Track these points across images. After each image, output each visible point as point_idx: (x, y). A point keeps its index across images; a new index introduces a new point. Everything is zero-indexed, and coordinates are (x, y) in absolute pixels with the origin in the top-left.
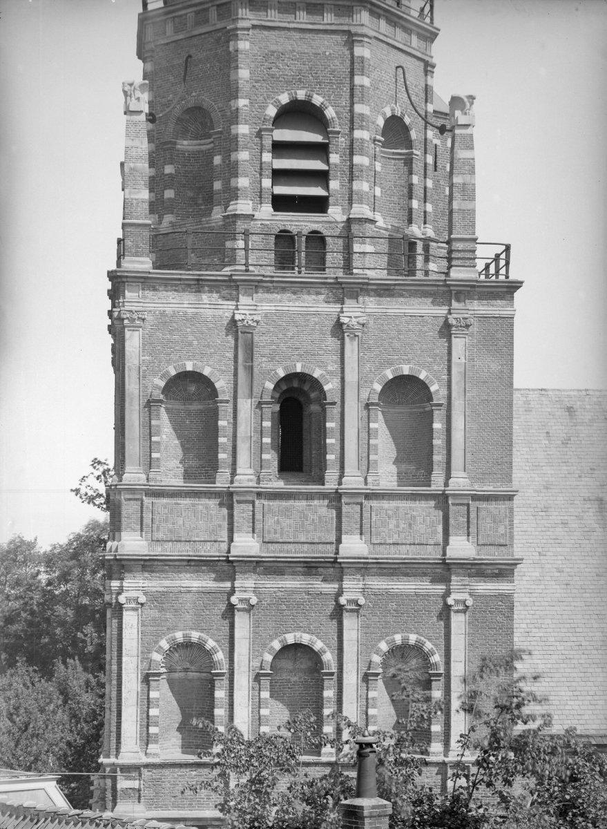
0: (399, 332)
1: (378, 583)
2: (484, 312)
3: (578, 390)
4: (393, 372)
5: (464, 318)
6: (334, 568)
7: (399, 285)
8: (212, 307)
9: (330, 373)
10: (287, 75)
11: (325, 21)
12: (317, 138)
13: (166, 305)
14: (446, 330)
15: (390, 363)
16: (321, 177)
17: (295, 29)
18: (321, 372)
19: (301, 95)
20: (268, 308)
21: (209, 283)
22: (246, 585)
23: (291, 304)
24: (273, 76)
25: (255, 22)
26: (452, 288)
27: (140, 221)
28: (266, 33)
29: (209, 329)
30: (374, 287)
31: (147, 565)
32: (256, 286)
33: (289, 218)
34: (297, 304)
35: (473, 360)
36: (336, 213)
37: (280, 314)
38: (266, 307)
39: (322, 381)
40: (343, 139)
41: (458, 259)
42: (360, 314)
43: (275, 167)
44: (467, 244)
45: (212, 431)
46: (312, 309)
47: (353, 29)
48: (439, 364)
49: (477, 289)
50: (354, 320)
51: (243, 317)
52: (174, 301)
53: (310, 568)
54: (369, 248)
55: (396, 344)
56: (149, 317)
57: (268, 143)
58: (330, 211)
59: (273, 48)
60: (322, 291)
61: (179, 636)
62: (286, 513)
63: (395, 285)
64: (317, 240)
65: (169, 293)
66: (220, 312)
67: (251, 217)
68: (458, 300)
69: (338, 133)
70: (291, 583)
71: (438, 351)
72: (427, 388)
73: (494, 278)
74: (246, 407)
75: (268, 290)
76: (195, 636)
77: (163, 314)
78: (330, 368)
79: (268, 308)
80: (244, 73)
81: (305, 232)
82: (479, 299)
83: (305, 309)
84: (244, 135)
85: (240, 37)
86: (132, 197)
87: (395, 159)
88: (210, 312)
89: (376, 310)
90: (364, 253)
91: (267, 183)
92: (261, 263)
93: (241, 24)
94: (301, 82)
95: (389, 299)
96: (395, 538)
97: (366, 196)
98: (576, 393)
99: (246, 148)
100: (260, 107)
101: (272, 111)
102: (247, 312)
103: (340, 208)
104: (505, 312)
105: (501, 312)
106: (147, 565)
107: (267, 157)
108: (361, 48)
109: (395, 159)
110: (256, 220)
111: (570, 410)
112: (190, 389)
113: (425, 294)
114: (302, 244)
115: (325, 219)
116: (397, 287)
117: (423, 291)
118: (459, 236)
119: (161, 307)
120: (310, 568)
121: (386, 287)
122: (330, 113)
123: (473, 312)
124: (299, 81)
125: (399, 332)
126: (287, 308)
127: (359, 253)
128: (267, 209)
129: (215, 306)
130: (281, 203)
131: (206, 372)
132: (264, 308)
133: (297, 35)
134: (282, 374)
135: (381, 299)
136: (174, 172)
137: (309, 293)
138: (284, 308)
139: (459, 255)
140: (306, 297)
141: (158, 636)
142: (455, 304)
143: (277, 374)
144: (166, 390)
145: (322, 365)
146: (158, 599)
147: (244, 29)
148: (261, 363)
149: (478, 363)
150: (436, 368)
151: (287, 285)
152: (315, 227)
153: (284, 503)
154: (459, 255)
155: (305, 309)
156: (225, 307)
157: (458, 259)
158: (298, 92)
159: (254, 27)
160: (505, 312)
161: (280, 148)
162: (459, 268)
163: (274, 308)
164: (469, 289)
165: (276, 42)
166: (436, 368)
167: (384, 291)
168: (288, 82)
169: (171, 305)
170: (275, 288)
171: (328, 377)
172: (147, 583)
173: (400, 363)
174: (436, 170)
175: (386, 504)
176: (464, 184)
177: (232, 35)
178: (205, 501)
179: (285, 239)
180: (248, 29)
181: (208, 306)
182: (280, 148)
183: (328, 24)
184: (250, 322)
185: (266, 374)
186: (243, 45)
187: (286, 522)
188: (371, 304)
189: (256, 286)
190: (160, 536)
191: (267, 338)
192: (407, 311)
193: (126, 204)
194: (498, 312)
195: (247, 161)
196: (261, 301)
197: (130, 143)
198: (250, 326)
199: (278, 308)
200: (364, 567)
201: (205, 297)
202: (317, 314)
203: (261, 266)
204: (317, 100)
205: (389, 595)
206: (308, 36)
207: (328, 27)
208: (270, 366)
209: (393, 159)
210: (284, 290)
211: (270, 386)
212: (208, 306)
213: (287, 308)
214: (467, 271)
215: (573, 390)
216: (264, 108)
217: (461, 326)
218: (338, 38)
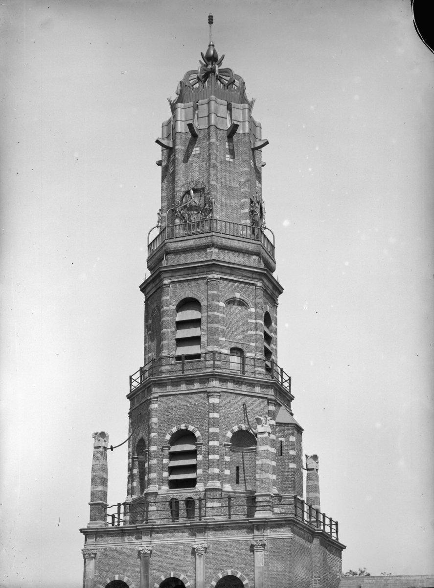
0: (226, 551)
2: (273, 536)
3: (422, 576)
4: (222, 574)
5: (260, 541)
7: (225, 524)
8: (129, 544)
9: (189, 577)
10: (176, 418)
11: (195, 388)
13: (107, 545)
14: (252, 548)
15: (221, 569)
17: (180, 394)
18: (184, 576)
19: (183, 427)
20: (157, 542)
21: (128, 531)
23: (169, 539)
24: (169, 419)
25: (160, 394)
26: (254, 524)
27: (96, 502)
28: (166, 398)
29: (128, 556)
30: (212, 526)
32: (151, 531)
33: (175, 492)
34: (172, 539)
35: (268, 564)
36: (200, 487)
37: (164, 545)
38: (156, 542)
39: (184, 582)
40: (204, 447)
41: (260, 506)
42: (203, 542)
43: (170, 465)
44: (264, 498)
46: (179, 541)
47: (208, 390)
48: (248, 568)
49: (268, 523)
50: (200, 545)
51: (143, 548)
52: (111, 543)
54: (155, 508)
55: (225, 558)
56: (99, 553)
57: (166, 453)
58: (196, 486)
59: (169, 405)
60: (185, 530)
63: (223, 524)
64: (190, 502)
65: (109, 538)
66: (133, 547)
67: (156, 494)
68: (258, 529)
69: (202, 444)
71: (248, 560)
72: (221, 580)
73: (110, 526)
75: (157, 533)
77: (105, 550)
78: (189, 574)
79: (157, 542)
80: (154, 420)
81: (184, 499)
82: (271, 528)
83: (176, 541)
84: (154, 451)
85: (153, 402)
86: (94, 490)
87: (249, 452)
88: (128, 547)
89: (214, 539)
90: (213, 507)
91: (165, 474)
92: (161, 517)
93: (154, 396)
94: (183, 420)
95: (220, 532)
98: (419, 578)
100: (163, 436)
101: (168, 437)
102: (145, 546)
103: (203, 483)
104: (285, 535)
105: (283, 536)
107: (166, 461)
108: (213, 399)
109: (249, 452)
110: (159, 495)
114: (182, 505)
115: (194, 490)
116: (224, 526)
117: (277, 524)
118: (260, 494)
119: (104, 546)
121: (218, 526)
123: (267, 537)
124: (183, 421)
125: (226, 551)
126: (166, 542)
127: (211, 508)
128: (165, 488)
129: (131, 543)
130: (174, 484)
132: (155, 542)
134: (163, 578)
135: (217, 532)
136: (296, 455)
137: (178, 532)
138: (164, 542)
139: (260, 504)
140: (176, 534)
143: (161, 579)
145: (185, 572)
147: (154, 398)
149: (271, 566)
150: (247, 570)
151: (167, 529)
152: (189, 495)
154: (260, 504)
155: (176, 541)
156: (136, 543)
157: (260, 506)
158: (182, 425)
159: (160, 396)
160: (285, 535)
161: (174, 456)
162: (260, 512)
163: (160, 542)
164: (263, 523)
165: (171, 402)
166: (247, 570)
168: (177, 421)
169: (109, 545)
170: (161, 531)
171: (187, 579)
173: (227, 569)
174: (282, 455)
176: (262, 464)
177: (149, 402)
179: (174, 504)
180: (157, 398)
181: (127, 544)
182: (174, 456)
183: (196, 389)
184: (146, 551)
186: (154, 406)
188: (211, 536)
189: (151, 531)
191: (156, 559)
192: (230, 538)
193: (92, 494)
194: (281, 535)
195: (156, 464)
196: (154, 539)
197: (95, 463)
198: (146, 553)
199: (163, 542)
201: (126, 539)
202: (182, 544)
203: (161, 519)
204: (191, 428)
206: (187, 396)
207: (196, 391)
208: (157, 575)
209: (249, 452)
210: (165, 532)
212: (127, 544)
213: (166, 542)
214: (264, 513)
215: (419, 576)
216: (164, 436)
217: (259, 545)
218: (202, 395)
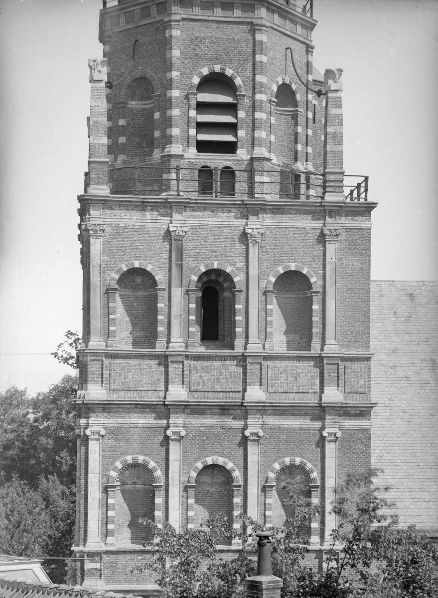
0: (288, 239)
1: (273, 421)
2: (349, 225)
3: (417, 282)
4: (283, 268)
5: (335, 230)
6: (241, 410)
7: (288, 205)
8: (153, 221)
9: (238, 269)
10: (207, 54)
11: (235, 15)
12: (229, 100)
13: (119, 220)
14: (322, 238)
15: (282, 262)
16: (232, 128)
17: (213, 21)
18: (232, 268)
19: (217, 68)
20: (194, 222)
21: (151, 204)
22: (178, 422)
23: (210, 219)
24: (197, 55)
25: (184, 16)
26: (326, 208)
27: (101, 160)
28: (192, 24)
29: (151, 237)
30: (270, 207)
31: (106, 407)
32: (185, 206)
33: (209, 157)
34: (214, 219)
35: (341, 259)
36: (242, 153)
37: (202, 227)
38: (192, 222)
39: (232, 275)
40: (248, 100)
41: (330, 187)
42: (260, 227)
43: (199, 120)
44: (337, 176)
45: (153, 311)
46: (225, 223)
47: (255, 21)
48: (317, 263)
49: (344, 209)
50: (255, 230)
51: (175, 229)
52: (126, 217)
53: (224, 409)
54: (266, 179)
55: (286, 248)
56: (107, 229)
57: (193, 103)
58: (238, 152)
59: (197, 34)
60: (233, 210)
61: (129, 459)
62: (207, 370)
63: (285, 205)
64: (229, 173)
65: (122, 212)
66: (159, 225)
67: (181, 157)
68: (331, 217)
69: (244, 96)
70: (210, 421)
71: (316, 253)
72: (308, 280)
73: (356, 201)
74: (177, 293)
75: (194, 209)
76: (141, 459)
77: (118, 226)
78: (238, 265)
79: (194, 222)
80: (176, 53)
81: (220, 167)
82: (346, 216)
83: (220, 223)
84: (176, 97)
85: (173, 26)
86: (95, 142)
87: (285, 115)
88: (151, 225)
89: (271, 224)
90: (263, 183)
91: (193, 132)
92: (188, 190)
93: (174, 17)
94: (217, 59)
95: (280, 216)
96: (285, 388)
97: (264, 141)
98: (415, 284)
99: (177, 106)
100: (188, 77)
101: (196, 80)
102: (179, 225)
103: (246, 150)
104: (365, 225)
105: (361, 225)
106: (106, 407)
107: (193, 113)
108: (261, 35)
109: (285, 115)
110: (185, 158)
111: (411, 296)
112: (137, 281)
113: (307, 212)
114: (218, 176)
115: (234, 158)
116: (286, 207)
117: (305, 210)
118: (331, 170)
119: (116, 222)
120: (224, 409)
121: (278, 207)
122: (238, 81)
123: (341, 225)
124: (216, 58)
125: (288, 239)
126: (207, 222)
127: (259, 183)
128: (193, 151)
129: (155, 221)
130: (202, 147)
131: (149, 268)
132: (191, 222)
133: (215, 25)
134: (203, 270)
135: (275, 216)
136: (125, 124)
137: (223, 212)
138: (205, 223)
139: (331, 184)
140: (221, 214)
141: (114, 459)
142: (328, 219)
143: (200, 270)
144: (120, 281)
145: (233, 263)
146: (114, 432)
147: (176, 21)
148: (188, 262)
149: (345, 262)
150: (314, 265)
151: (207, 206)
152: (227, 164)
153: (205, 363)
154: (331, 184)
155: (220, 223)
156: (162, 221)
157: (330, 187)
158: (215, 66)
159: (183, 19)
160: (365, 225)
161: (202, 107)
162: (331, 193)
163: (198, 222)
164: (338, 208)
165: (199, 30)
166: (314, 265)
167: (277, 210)
168: (208, 59)
169: (123, 220)
170: (199, 208)
171: (237, 272)
172: (106, 421)
173: (289, 262)
174: (314, 123)
175: (278, 364)
176: (335, 133)
177: (167, 25)
178: (148, 361)
179: (205, 172)
180: (179, 21)
181: (150, 221)
182: (202, 107)
183: (237, 17)
184: (180, 233)
185: (192, 270)
186: (176, 33)
187: (206, 377)
188: (268, 220)
189: (185, 206)
190: (115, 386)
191: (192, 244)
192: (293, 224)
193: (91, 147)
194: (359, 225)
195: (179, 116)
196: (188, 217)
197: (94, 103)
198: (180, 235)
199: (201, 222)
200: (262, 409)
201: (148, 215)
202: (228, 226)
203: (188, 192)
204: (229, 72)
205: (281, 429)
206: (222, 26)
207: (237, 20)
208: (195, 264)
209: (284, 114)
210: (205, 209)
211: (195, 278)
212: (150, 221)
213: (207, 222)
214: (337, 196)
215: (414, 281)
216: (191, 78)
217: (333, 235)
218: (244, 27)
